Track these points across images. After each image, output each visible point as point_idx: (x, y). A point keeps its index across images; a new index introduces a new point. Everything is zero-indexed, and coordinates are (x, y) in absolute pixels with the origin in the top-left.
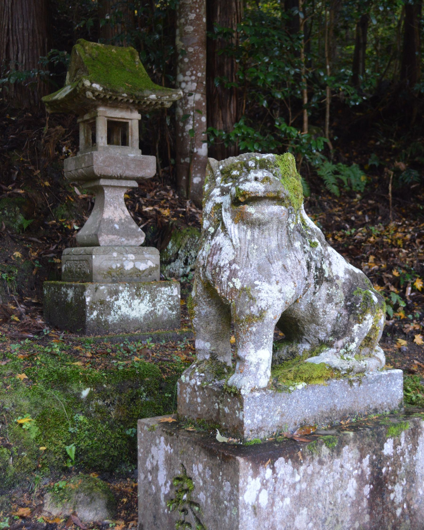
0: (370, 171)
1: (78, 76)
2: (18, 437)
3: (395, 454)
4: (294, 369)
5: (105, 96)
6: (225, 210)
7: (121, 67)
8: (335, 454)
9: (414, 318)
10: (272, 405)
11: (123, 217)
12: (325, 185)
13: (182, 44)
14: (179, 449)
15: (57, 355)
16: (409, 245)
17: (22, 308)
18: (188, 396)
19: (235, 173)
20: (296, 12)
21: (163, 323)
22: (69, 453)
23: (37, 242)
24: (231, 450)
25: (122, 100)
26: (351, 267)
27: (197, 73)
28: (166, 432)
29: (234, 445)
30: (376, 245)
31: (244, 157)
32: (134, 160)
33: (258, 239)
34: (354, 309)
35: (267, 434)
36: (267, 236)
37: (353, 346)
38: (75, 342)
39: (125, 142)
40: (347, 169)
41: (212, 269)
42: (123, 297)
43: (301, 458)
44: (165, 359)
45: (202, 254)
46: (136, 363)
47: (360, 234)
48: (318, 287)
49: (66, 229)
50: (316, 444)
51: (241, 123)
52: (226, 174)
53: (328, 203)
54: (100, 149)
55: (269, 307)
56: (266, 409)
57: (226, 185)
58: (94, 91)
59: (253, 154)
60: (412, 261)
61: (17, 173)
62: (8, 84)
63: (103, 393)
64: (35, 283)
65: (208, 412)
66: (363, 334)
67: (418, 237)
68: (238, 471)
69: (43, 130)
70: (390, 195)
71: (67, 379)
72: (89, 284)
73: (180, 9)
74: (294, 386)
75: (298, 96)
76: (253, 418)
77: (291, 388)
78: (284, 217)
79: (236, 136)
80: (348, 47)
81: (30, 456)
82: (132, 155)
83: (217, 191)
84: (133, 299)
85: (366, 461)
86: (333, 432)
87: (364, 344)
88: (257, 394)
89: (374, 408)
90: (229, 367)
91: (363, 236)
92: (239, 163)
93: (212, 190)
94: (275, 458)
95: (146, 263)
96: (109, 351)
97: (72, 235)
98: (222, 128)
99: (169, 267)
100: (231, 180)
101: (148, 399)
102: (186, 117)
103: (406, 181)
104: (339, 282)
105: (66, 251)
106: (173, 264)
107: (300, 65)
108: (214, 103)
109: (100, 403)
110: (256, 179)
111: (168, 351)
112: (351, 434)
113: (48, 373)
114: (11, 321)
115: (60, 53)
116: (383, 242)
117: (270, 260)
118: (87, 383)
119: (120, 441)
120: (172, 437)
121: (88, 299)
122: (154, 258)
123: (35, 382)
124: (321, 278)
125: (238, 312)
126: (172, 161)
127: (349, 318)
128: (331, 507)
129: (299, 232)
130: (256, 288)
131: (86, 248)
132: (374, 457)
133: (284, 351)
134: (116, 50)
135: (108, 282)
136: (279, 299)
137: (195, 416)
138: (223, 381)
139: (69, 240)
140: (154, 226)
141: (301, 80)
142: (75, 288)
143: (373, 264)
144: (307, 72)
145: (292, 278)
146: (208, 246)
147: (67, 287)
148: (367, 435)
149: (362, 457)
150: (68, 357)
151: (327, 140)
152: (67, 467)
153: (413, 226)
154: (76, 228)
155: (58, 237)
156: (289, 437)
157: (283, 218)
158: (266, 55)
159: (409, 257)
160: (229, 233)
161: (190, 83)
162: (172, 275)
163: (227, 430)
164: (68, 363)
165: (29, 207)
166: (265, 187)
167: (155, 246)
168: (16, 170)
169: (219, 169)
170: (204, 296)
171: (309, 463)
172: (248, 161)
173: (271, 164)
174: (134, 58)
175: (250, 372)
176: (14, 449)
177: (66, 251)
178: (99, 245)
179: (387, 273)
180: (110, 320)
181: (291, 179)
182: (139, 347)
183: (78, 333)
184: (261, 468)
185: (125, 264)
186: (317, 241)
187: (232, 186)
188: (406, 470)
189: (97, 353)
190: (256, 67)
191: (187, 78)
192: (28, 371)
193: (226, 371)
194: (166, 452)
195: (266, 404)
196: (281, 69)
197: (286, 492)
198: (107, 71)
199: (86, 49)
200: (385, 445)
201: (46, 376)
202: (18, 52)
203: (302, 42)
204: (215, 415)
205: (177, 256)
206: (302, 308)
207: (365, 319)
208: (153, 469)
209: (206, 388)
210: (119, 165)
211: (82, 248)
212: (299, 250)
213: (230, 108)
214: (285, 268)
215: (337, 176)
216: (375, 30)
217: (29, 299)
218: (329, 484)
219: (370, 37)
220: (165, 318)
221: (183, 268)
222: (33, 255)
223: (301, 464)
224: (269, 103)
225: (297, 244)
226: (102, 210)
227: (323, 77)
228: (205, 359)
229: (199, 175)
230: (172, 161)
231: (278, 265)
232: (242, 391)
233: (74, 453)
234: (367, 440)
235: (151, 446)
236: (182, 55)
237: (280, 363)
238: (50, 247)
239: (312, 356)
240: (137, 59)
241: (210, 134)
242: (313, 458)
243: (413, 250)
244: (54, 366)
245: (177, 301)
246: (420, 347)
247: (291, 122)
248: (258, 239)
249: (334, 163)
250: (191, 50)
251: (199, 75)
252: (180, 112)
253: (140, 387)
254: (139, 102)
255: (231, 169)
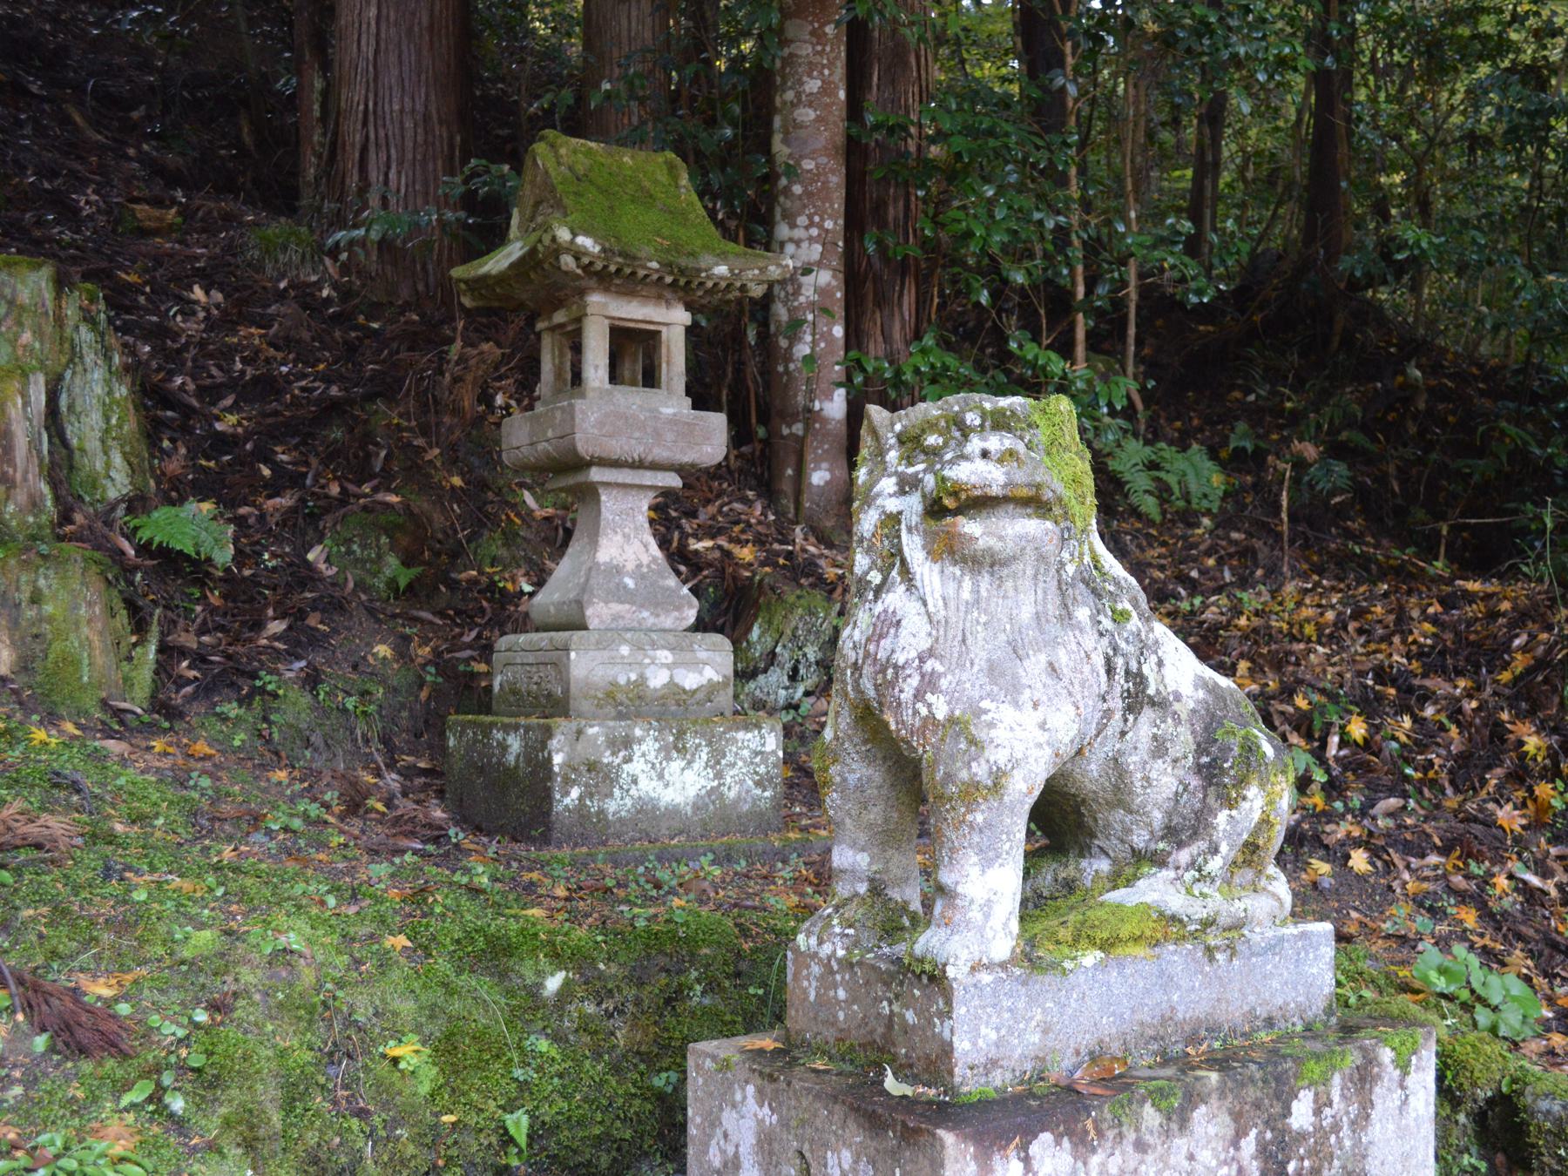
0: (1234, 463)
1: (540, 219)
2: (386, 1091)
3: (1319, 1128)
4: (1073, 918)
5: (605, 267)
6: (910, 530)
7: (645, 198)
8: (1174, 1126)
9: (1348, 810)
10: (1021, 1005)
11: (645, 560)
12: (1126, 496)
13: (786, 150)
14: (793, 1113)
15: (483, 891)
16: (1331, 636)
17: (392, 780)
18: (814, 984)
19: (932, 440)
20: (1060, 81)
21: (739, 817)
22: (512, 1131)
23: (431, 623)
24: (922, 1115)
25: (646, 276)
26: (1209, 673)
27: (822, 220)
28: (761, 1073)
29: (930, 1103)
30: (1252, 635)
31: (954, 402)
32: (673, 421)
33: (988, 599)
34: (1217, 773)
35: (1009, 1076)
36: (1011, 593)
37: (1215, 865)
38: (525, 863)
39: (650, 379)
40: (1180, 456)
41: (877, 673)
42: (644, 755)
43: (1092, 1133)
44: (749, 903)
45: (851, 637)
46: (678, 912)
47: (1214, 609)
48: (1131, 718)
49: (503, 591)
50: (1130, 1102)
51: (929, 340)
52: (911, 443)
53: (1134, 537)
54: (590, 394)
55: (1016, 764)
56: (1007, 1015)
57: (911, 470)
59: (976, 396)
60: (1340, 674)
61: (383, 454)
62: (363, 243)
63: (599, 984)
64: (426, 722)
65: (864, 1022)
66: (1240, 835)
67: (1354, 617)
68: (942, 1166)
69: (447, 353)
70: (1284, 516)
71: (509, 950)
72: (560, 721)
73: (783, 68)
74: (1075, 958)
75: (1062, 282)
76: (975, 1034)
77: (1068, 965)
78: (1051, 548)
79: (917, 371)
80: (1177, 173)
81: (417, 1139)
82: (668, 411)
83: (888, 485)
84: (668, 758)
85: (1249, 1145)
86: (1170, 1071)
87: (1240, 860)
88: (986, 978)
89: (1265, 1015)
90: (915, 913)
91: (1222, 614)
92: (941, 416)
93: (878, 481)
94: (1029, 1135)
95: (701, 673)
96: (610, 883)
97: (517, 606)
98: (881, 354)
99: (752, 685)
100: (922, 457)
101: (707, 1001)
102: (796, 325)
103: (1319, 487)
104: (1183, 709)
105: (503, 642)
106: (761, 678)
107: (1068, 209)
108: (861, 293)
109: (590, 1008)
110: (985, 454)
111: (753, 887)
112: (1214, 1077)
113: (461, 935)
114: (366, 812)
115: (494, 168)
116: (1270, 627)
117: (1017, 652)
118: (558, 958)
119: (637, 1102)
120: (773, 1086)
121: (558, 759)
122: (719, 659)
123: (430, 955)
124: (1137, 698)
125: (939, 775)
126: (761, 432)
127: (1205, 796)
129: (1087, 585)
130: (984, 717)
131: (553, 634)
132: (1269, 1135)
133: (1046, 877)
134: (632, 157)
135: (606, 717)
136: (1039, 746)
137: (830, 1034)
138: (900, 949)
139: (509, 617)
140: (716, 587)
141: (1070, 244)
142: (526, 732)
143: (1247, 682)
144: (1084, 225)
145: (1070, 694)
146: (867, 615)
147: (506, 729)
148: (1252, 1080)
149: (1240, 1134)
150: (511, 897)
151: (1133, 386)
152: (507, 1167)
153: (1340, 591)
154: (527, 588)
155: (482, 610)
156: (1063, 1083)
157: (1050, 548)
158: (986, 180)
159: (1333, 665)
160: (918, 584)
161: (805, 245)
162: (759, 705)
163: (911, 1066)
164: (513, 912)
165: (414, 539)
166: (1007, 474)
167: (720, 630)
168: (382, 447)
169: (892, 431)
170: (856, 740)
171: (1113, 1148)
172: (963, 411)
173: (1019, 420)
174: (675, 178)
175: (968, 922)
176: (377, 1120)
177: (503, 642)
178: (586, 628)
179: (1282, 702)
180: (611, 810)
181: (1067, 456)
182: (682, 876)
183: (533, 840)
184: (996, 1157)
185: (648, 673)
186: (1128, 607)
187: (925, 471)
188: (1344, 1167)
189: (581, 888)
190: (964, 208)
191: (799, 233)
192: (413, 929)
193: (907, 924)
194: (760, 1122)
195: (1007, 1003)
196: (1023, 215)
198: (611, 208)
199: (558, 155)
200: (1295, 1105)
201: (458, 942)
202: (389, 167)
203: (1072, 152)
204: (881, 1030)
205: (772, 657)
206: (1093, 769)
207: (1244, 798)
208: (725, 1165)
209: (860, 963)
210: (637, 435)
211: (545, 635)
212: (1088, 628)
213: (900, 306)
214: (1052, 668)
215: (1156, 473)
216: (1242, 133)
217: (410, 759)
219: (1228, 149)
220: (746, 807)
221: (786, 688)
222: (420, 652)
223: (1094, 1150)
224: (994, 295)
225: (1083, 614)
226: (594, 544)
227: (1124, 236)
228: (856, 894)
229: (824, 465)
230: (761, 432)
231: (1038, 662)
232: (948, 968)
233: (525, 1131)
234: (1252, 1093)
235: (721, 1109)
236: (788, 177)
237: (1036, 907)
238: (462, 634)
239: (1115, 888)
240: (684, 180)
241: (854, 366)
242: (1121, 1135)
243: (1343, 649)
244: (477, 918)
245: (775, 766)
246: (1361, 878)
247: (1046, 342)
248: (988, 599)
249: (1147, 443)
250: (808, 165)
251: (829, 224)
252: (781, 312)
253: (687, 970)
254: (688, 283)
255: (923, 431)
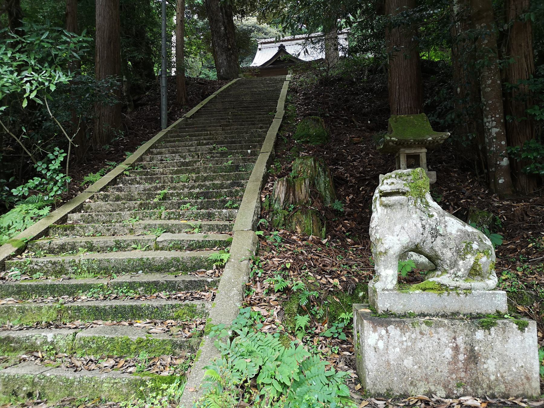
58: (393, 141)
88: (386, 292)
126: (486, 171)
128: (432, 361)
197: (397, 344)
218: (429, 347)
230: (486, 171)
